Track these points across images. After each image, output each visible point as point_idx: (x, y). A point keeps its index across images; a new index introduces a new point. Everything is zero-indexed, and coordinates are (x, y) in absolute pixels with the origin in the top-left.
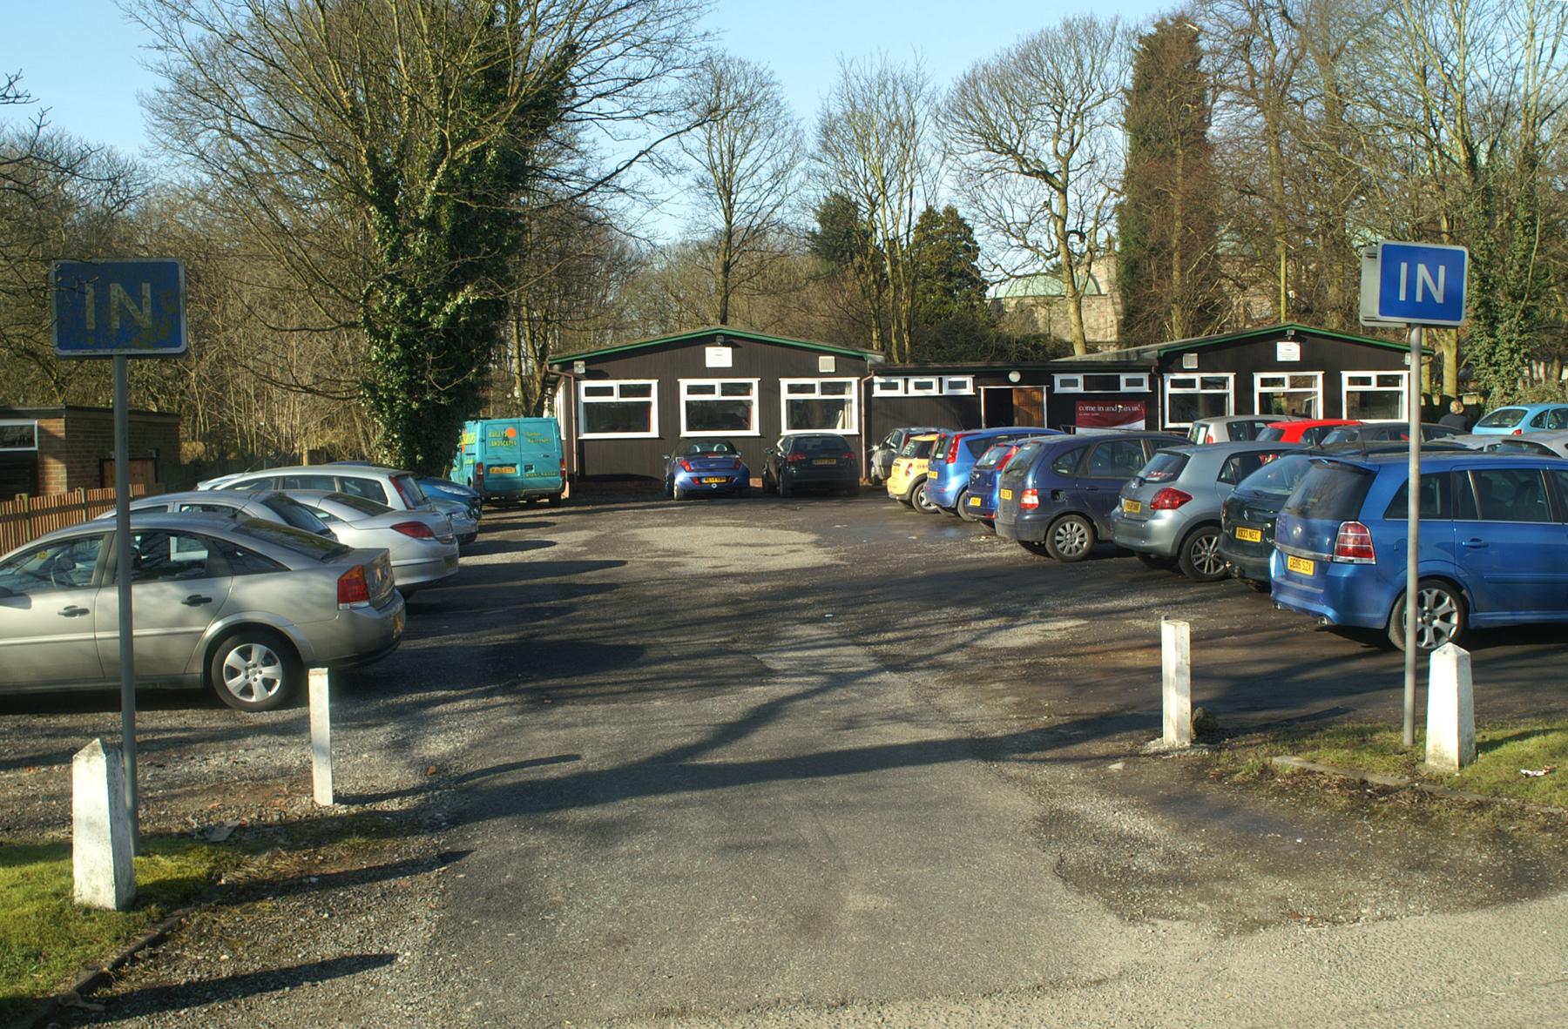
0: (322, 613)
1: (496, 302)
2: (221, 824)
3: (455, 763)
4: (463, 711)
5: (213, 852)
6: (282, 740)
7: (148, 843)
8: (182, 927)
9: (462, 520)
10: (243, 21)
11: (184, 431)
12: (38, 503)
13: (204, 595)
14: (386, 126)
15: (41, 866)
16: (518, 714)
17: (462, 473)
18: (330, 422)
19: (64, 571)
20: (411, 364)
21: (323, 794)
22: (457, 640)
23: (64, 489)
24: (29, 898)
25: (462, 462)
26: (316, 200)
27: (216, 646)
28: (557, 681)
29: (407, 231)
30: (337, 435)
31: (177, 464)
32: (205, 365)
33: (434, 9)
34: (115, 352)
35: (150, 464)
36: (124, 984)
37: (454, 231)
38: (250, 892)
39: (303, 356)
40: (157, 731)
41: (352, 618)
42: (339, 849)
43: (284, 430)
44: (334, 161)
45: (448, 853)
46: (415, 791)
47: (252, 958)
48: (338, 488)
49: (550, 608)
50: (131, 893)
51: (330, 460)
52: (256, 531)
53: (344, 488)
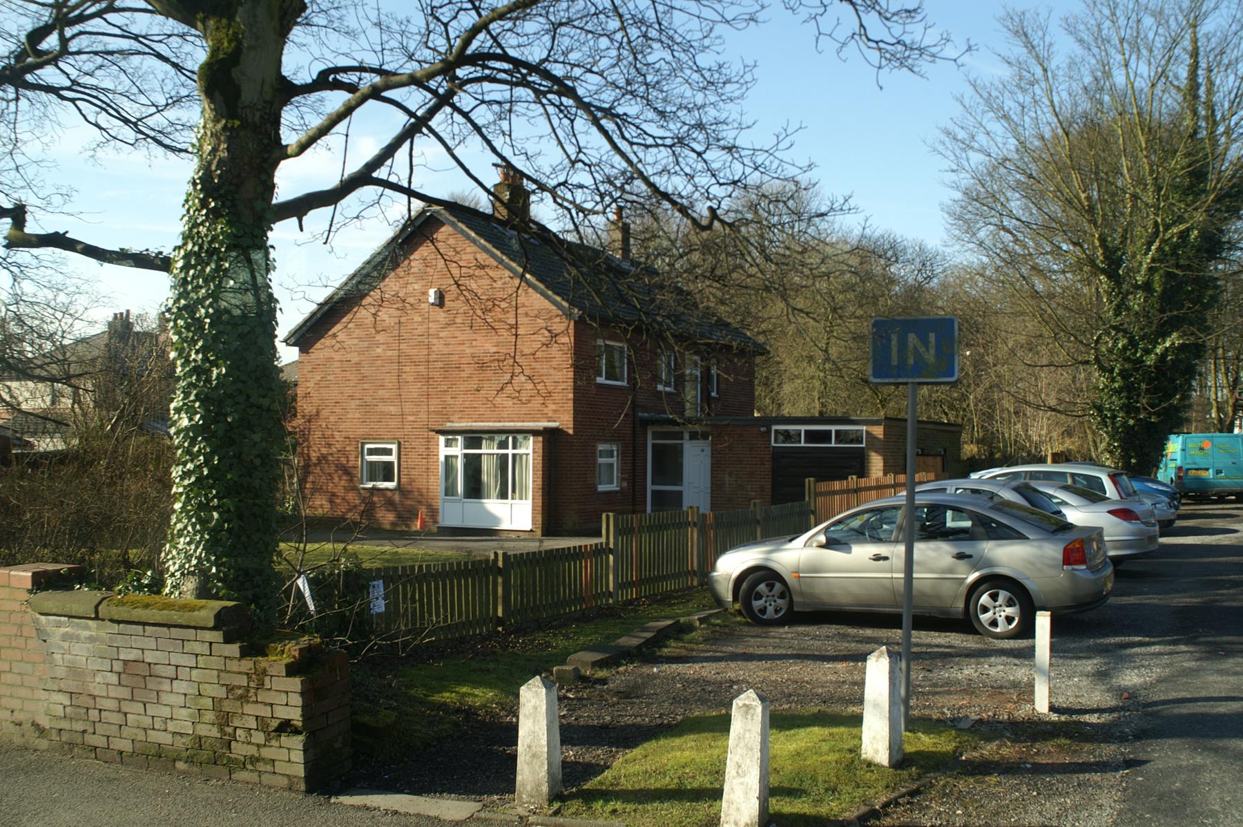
0: (1052, 572)
1: (1196, 345)
2: (967, 717)
3: (1143, 692)
4: (1154, 654)
5: (959, 736)
6: (1016, 661)
7: (913, 724)
8: (932, 786)
9: (1163, 509)
10: (1012, 148)
11: (965, 436)
12: (863, 482)
13: (968, 552)
14: (1114, 216)
15: (842, 729)
16: (1197, 660)
17: (1166, 473)
18: (1069, 433)
19: (874, 529)
20: (1129, 392)
21: (1041, 704)
22: (1154, 600)
23: (881, 474)
24: (832, 750)
25: (1166, 465)
26: (1064, 272)
27: (974, 588)
28: (1230, 638)
29: (1128, 293)
30: (1073, 443)
31: (957, 458)
32: (980, 390)
33: (1150, 129)
34: (910, 380)
35: (939, 459)
36: (889, 820)
37: (1164, 291)
38: (982, 768)
39: (1049, 386)
40: (929, 646)
41: (1073, 577)
42: (1049, 746)
43: (1035, 438)
44: (1075, 244)
45: (1131, 760)
46: (1111, 710)
47: (979, 816)
48: (1070, 481)
49: (1229, 581)
50: (899, 757)
51: (1068, 460)
52: (1006, 509)
53: (1074, 481)
